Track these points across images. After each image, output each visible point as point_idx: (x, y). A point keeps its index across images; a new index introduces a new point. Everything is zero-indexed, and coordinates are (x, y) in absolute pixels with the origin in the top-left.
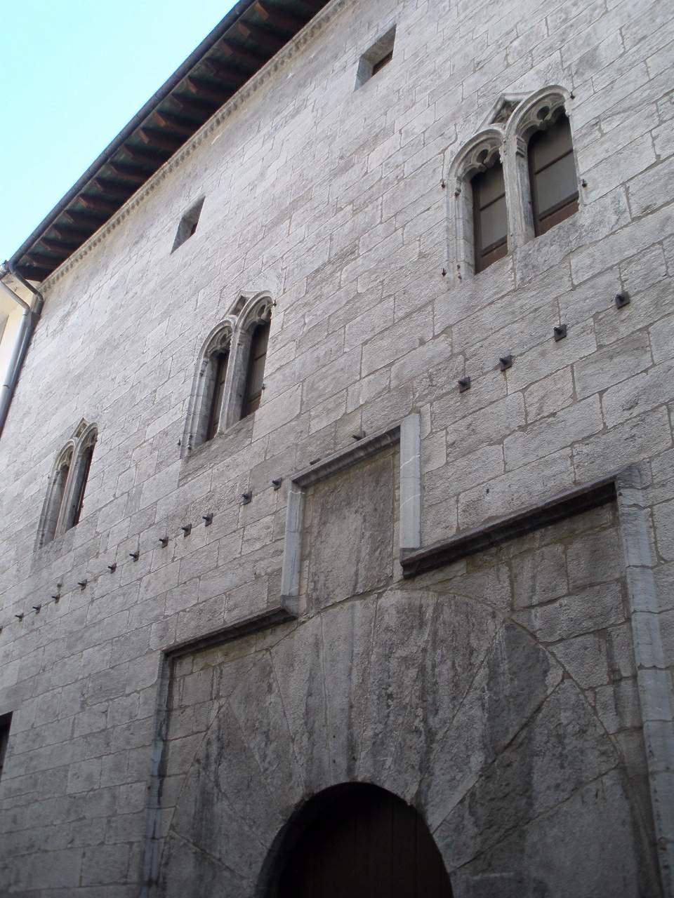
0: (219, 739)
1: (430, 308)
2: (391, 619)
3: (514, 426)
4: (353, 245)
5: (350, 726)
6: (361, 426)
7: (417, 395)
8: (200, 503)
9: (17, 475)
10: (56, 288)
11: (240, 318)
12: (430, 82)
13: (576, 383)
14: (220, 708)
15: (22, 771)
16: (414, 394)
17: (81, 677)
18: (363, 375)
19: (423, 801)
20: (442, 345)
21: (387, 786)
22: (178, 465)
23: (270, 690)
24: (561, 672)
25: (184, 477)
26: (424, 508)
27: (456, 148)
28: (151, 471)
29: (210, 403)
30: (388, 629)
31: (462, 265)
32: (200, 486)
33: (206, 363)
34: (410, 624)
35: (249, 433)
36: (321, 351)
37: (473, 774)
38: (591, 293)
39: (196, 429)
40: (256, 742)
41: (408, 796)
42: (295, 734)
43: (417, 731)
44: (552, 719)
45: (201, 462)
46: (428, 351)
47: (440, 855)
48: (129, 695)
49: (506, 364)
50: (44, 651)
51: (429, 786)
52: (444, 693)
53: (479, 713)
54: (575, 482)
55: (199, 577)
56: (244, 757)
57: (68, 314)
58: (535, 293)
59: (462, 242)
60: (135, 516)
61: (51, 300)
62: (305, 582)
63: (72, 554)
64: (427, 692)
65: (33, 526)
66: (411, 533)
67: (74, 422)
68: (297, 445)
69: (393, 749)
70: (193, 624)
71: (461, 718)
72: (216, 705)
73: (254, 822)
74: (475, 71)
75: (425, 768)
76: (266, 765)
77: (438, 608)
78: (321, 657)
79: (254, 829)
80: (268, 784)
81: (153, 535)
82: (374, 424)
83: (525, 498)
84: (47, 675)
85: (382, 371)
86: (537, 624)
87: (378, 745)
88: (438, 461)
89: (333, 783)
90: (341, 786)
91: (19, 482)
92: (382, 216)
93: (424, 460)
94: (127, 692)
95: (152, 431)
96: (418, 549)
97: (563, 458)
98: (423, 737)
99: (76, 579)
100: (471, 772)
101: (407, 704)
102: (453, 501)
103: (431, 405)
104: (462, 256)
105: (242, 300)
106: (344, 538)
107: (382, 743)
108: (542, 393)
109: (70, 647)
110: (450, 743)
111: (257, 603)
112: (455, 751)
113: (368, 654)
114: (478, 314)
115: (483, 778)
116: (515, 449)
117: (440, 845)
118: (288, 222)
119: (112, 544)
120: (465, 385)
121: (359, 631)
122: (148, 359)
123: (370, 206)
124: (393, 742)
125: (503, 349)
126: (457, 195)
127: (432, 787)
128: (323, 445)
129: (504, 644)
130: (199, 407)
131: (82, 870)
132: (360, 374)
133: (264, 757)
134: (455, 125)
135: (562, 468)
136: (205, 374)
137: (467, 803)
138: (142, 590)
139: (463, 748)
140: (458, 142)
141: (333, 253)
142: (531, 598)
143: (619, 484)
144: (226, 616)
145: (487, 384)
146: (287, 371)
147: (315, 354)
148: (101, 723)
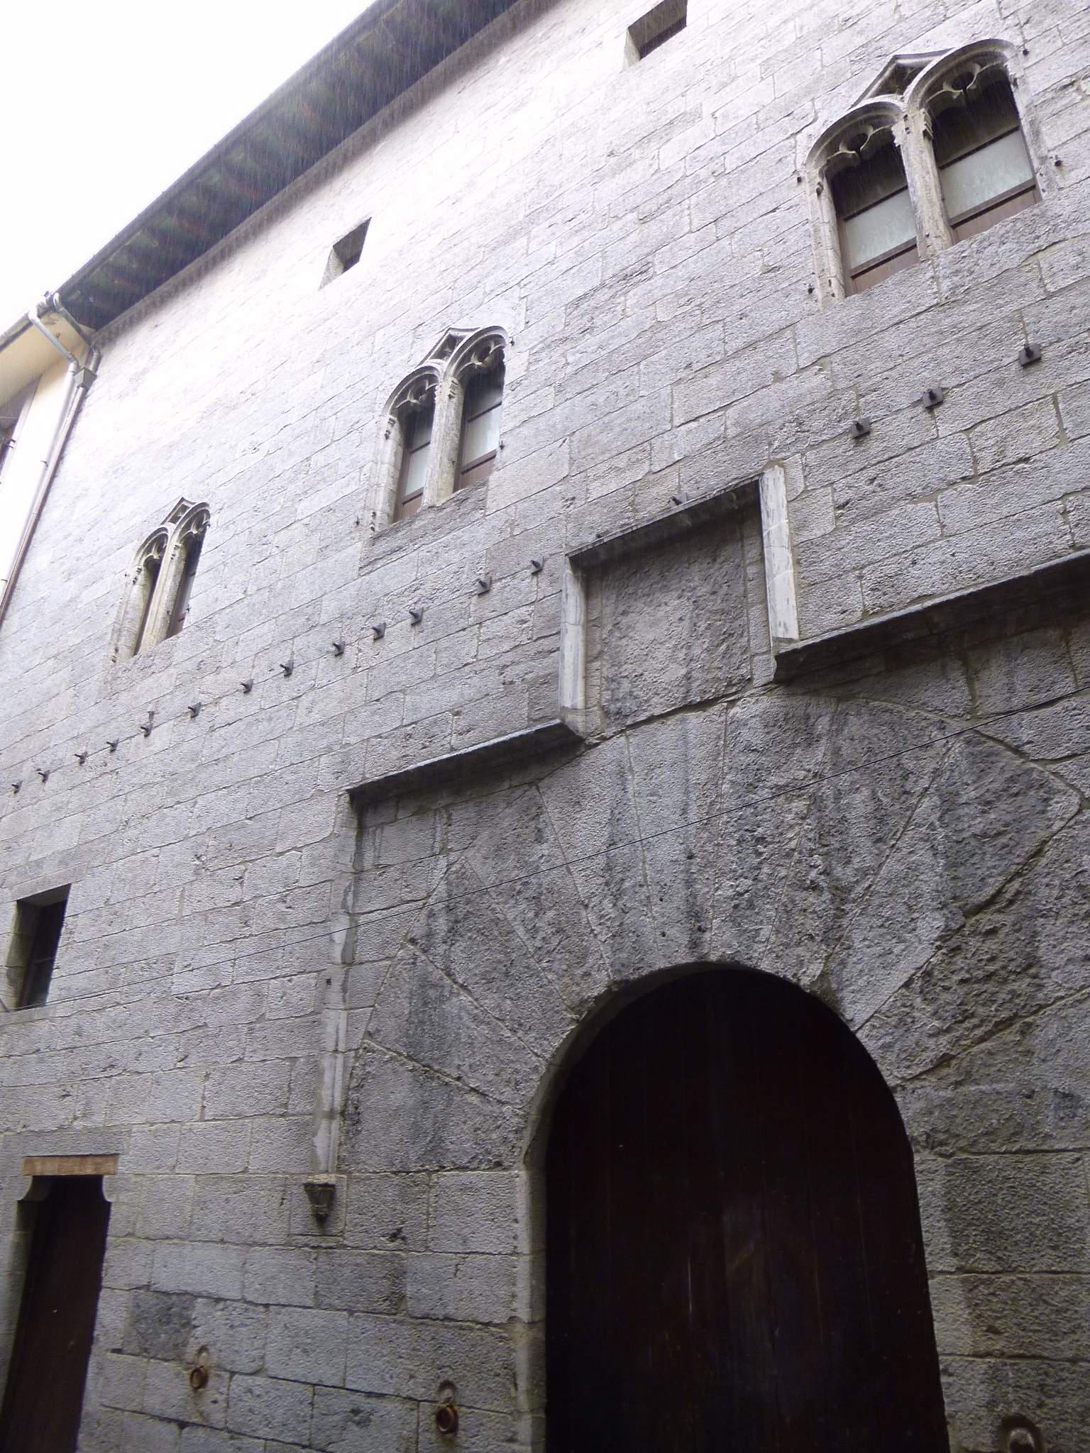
0: (449, 909)
1: (788, 334)
2: (754, 735)
4: (643, 262)
5: (689, 883)
6: (680, 486)
7: (776, 444)
8: (399, 595)
9: (69, 575)
11: (452, 363)
12: (761, 50)
13: (1064, 419)
14: (449, 865)
16: (770, 444)
17: (193, 833)
18: (677, 422)
19: (834, 986)
20: (815, 382)
21: (766, 966)
22: (356, 549)
24: (1076, 800)
25: (369, 564)
26: (805, 588)
27: (819, 129)
29: (397, 475)
30: (749, 749)
31: (834, 281)
33: (392, 422)
34: (789, 742)
35: (481, 505)
36: (600, 396)
37: (926, 944)
40: (514, 912)
41: (808, 975)
42: (589, 898)
43: (814, 887)
44: (1066, 865)
45: (399, 543)
46: (792, 388)
47: (871, 1064)
48: (281, 854)
49: (934, 401)
50: (126, 800)
51: (843, 963)
52: (859, 832)
53: (928, 858)
54: (1073, 547)
55: (403, 691)
56: (496, 933)
58: (976, 306)
60: (283, 617)
62: (595, 691)
63: (172, 670)
64: (829, 836)
68: (568, 516)
69: (773, 913)
70: (395, 754)
71: (892, 866)
72: (443, 863)
73: (520, 1025)
74: (840, 31)
75: (833, 936)
76: (538, 944)
78: (630, 790)
79: (520, 1033)
80: (544, 969)
81: (324, 640)
83: (982, 567)
84: (132, 833)
85: (709, 417)
87: (743, 907)
88: (822, 525)
91: (72, 583)
92: (691, 224)
93: (798, 526)
94: (278, 850)
95: (308, 507)
96: (796, 641)
97: (1053, 516)
98: (826, 896)
99: (181, 702)
100: (920, 942)
101: (794, 850)
102: (851, 577)
103: (803, 455)
106: (663, 632)
107: (751, 905)
110: (877, 902)
111: (510, 722)
112: (887, 913)
113: (716, 785)
114: (876, 337)
115: (944, 951)
116: (960, 502)
117: (871, 1046)
118: (524, 240)
120: (861, 433)
121: (698, 753)
122: (293, 418)
123: (670, 212)
124: (772, 904)
125: (928, 378)
126: (819, 193)
127: (850, 966)
128: (612, 514)
129: (964, 765)
131: (204, 1098)
132: (671, 421)
134: (813, 100)
135: (1048, 528)
136: (391, 436)
137: (917, 985)
138: (302, 711)
139: (904, 909)
140: (820, 121)
141: (610, 273)
142: (1008, 700)
144: (454, 740)
146: (542, 423)
147: (591, 399)
148: (235, 894)
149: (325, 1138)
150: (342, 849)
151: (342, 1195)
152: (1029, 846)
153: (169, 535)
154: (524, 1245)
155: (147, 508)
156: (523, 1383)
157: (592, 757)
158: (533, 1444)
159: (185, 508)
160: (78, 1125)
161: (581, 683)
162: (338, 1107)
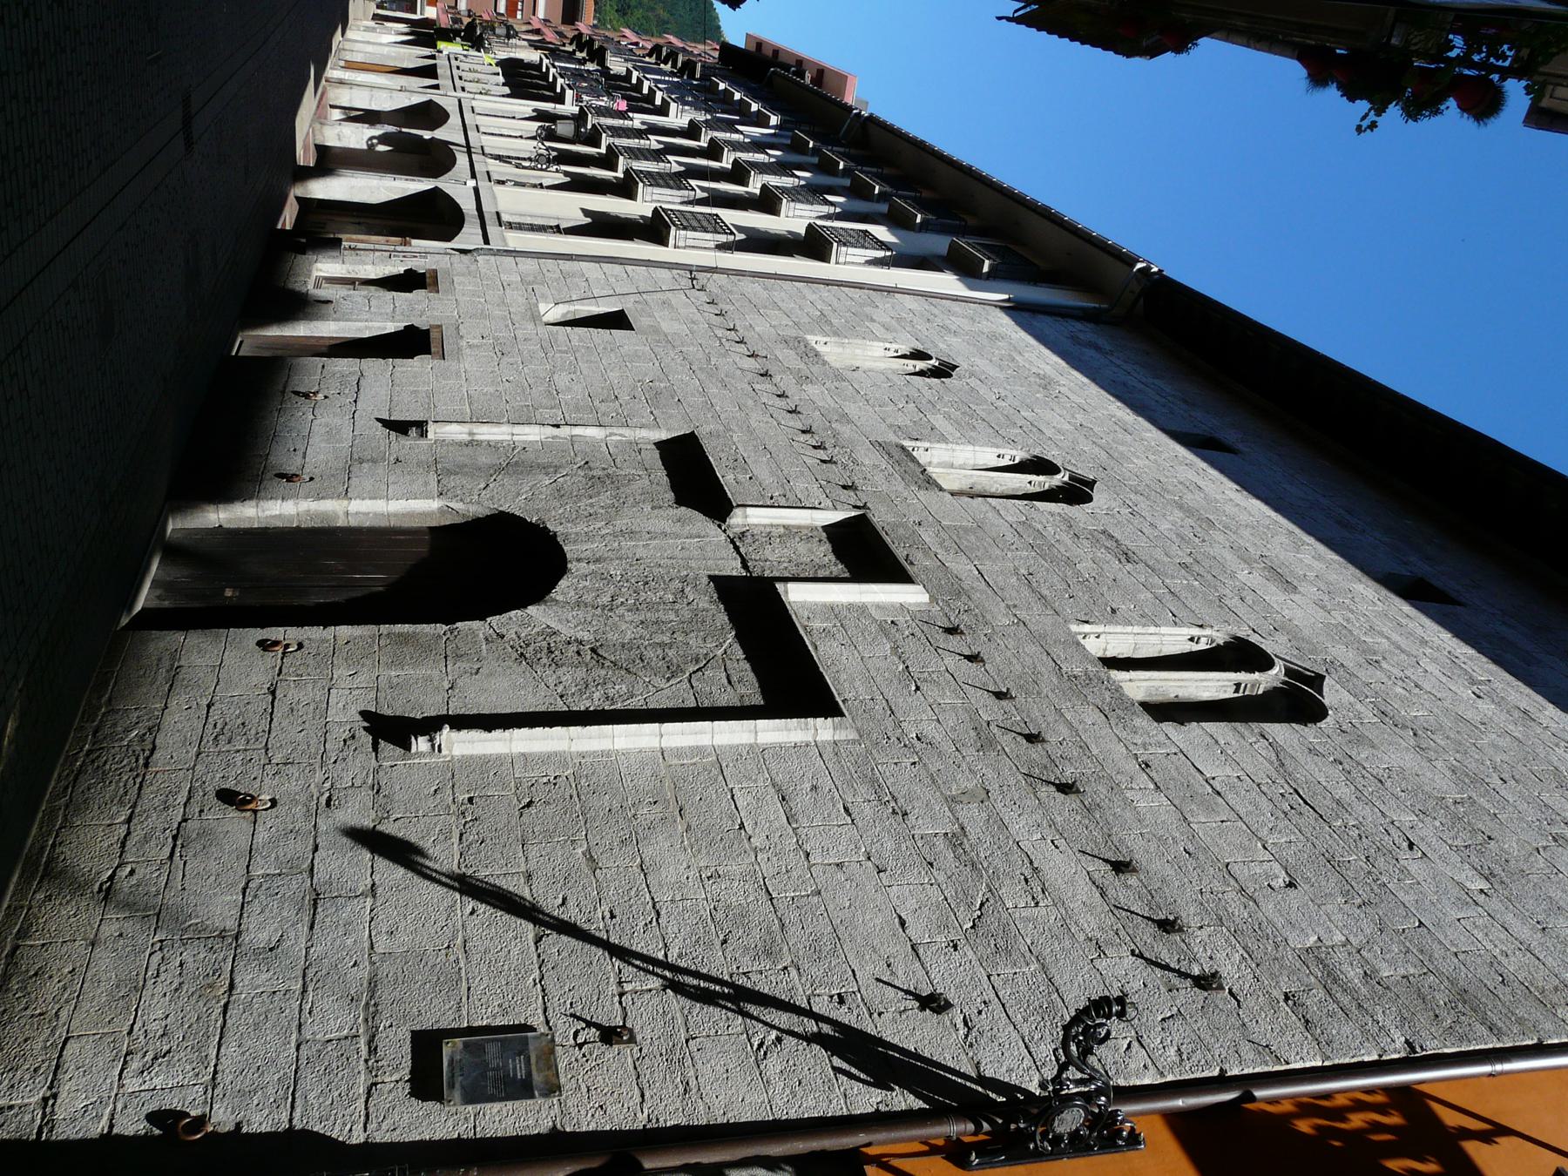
3: (908, 663)
25: (880, 446)
38: (1050, 719)
57: (1097, 348)
82: (919, 563)
133: (592, 505)
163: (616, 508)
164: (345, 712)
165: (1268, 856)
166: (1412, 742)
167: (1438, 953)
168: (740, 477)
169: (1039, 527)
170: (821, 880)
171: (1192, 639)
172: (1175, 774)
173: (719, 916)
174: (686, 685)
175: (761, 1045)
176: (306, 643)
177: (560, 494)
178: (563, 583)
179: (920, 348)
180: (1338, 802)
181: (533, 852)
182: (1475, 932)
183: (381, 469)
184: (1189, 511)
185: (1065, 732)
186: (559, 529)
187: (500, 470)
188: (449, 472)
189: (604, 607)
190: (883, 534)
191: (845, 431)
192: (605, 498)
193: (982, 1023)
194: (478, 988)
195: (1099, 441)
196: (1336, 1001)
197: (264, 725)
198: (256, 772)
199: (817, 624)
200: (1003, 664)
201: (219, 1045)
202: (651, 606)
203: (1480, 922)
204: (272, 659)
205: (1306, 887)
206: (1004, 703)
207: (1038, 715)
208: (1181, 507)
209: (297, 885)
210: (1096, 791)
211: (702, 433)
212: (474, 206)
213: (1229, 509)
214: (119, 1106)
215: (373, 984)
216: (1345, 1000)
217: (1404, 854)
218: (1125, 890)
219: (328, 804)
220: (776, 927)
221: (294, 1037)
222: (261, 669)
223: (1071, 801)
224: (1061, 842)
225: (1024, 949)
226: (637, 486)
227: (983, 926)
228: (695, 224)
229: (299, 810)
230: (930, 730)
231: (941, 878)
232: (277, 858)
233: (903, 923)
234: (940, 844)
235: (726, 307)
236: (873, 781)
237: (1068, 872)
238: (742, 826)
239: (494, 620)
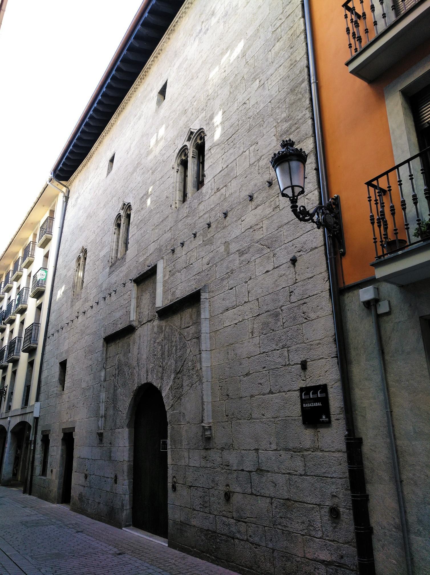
3: (183, 267)
10: (73, 184)
15: (70, 380)
23: (129, 352)
25: (110, 273)
26: (164, 292)
28: (101, 271)
31: (177, 202)
32: (114, 278)
38: (202, 220)
39: (113, 255)
57: (77, 198)
59: (178, 192)
61: (72, 189)
65: (70, 288)
66: (160, 303)
67: (81, 247)
77: (166, 326)
82: (150, 262)
84: (76, 345)
86: (186, 334)
89: (143, 383)
90: (145, 384)
95: (102, 254)
104: (178, 198)
105: (124, 204)
108: (189, 256)
109: (81, 335)
119: (91, 297)
126: (177, 172)
130: (114, 246)
133: (128, 374)
143: (201, 291)
145: (178, 250)
149: (101, 423)
150: (103, 353)
151: (104, 435)
152: (184, 359)
153: (189, 147)
154: (127, 444)
155: (75, 251)
156: (126, 474)
157: (138, 332)
158: (129, 486)
159: (192, 133)
160: (69, 420)
161: (135, 313)
162: (103, 415)
163: (127, 364)
164: (195, 459)
165: (247, 152)
166: (212, 100)
167: (279, 97)
168: (119, 323)
169: (139, 221)
170: (254, 298)
171: (177, 172)
172: (221, 180)
173: (264, 332)
174: (189, 342)
175: (306, 319)
176: (174, 475)
177: (124, 385)
178: (154, 384)
179: (75, 259)
180: (231, 127)
181: (245, 394)
182: (273, 84)
183: (113, 449)
184: (135, 170)
185: (207, 215)
186: (136, 385)
187: (115, 407)
188: (115, 424)
189: (163, 370)
190: (140, 274)
191: (104, 286)
192: (126, 369)
193: (299, 246)
194: (288, 413)
195: (110, 199)
196: (294, 131)
197: (201, 489)
198: (217, 492)
199: (170, 297)
200: (184, 234)
201: (307, 503)
202: (163, 354)
203: (269, 83)
204: (179, 487)
205: (258, 139)
206: (197, 235)
207: (202, 224)
208: (133, 173)
209: (255, 477)
210: (226, 207)
211: (104, 336)
212: (18, 417)
213: (134, 156)
214: (328, 538)
215: (287, 449)
216: (293, 128)
217: (247, 106)
218: (259, 198)
219: (228, 466)
220: (269, 313)
221: (305, 477)
222: (182, 491)
223: (230, 214)
224: (243, 218)
225: (276, 232)
226: (122, 359)
227: (269, 244)
228: (29, 337)
229: (230, 476)
230: (205, 260)
231: (254, 258)
232: (246, 484)
233: (267, 272)
234: (242, 258)
235: (60, 327)
236: (222, 280)
237: (251, 217)
238: (236, 324)
239: (167, 408)
